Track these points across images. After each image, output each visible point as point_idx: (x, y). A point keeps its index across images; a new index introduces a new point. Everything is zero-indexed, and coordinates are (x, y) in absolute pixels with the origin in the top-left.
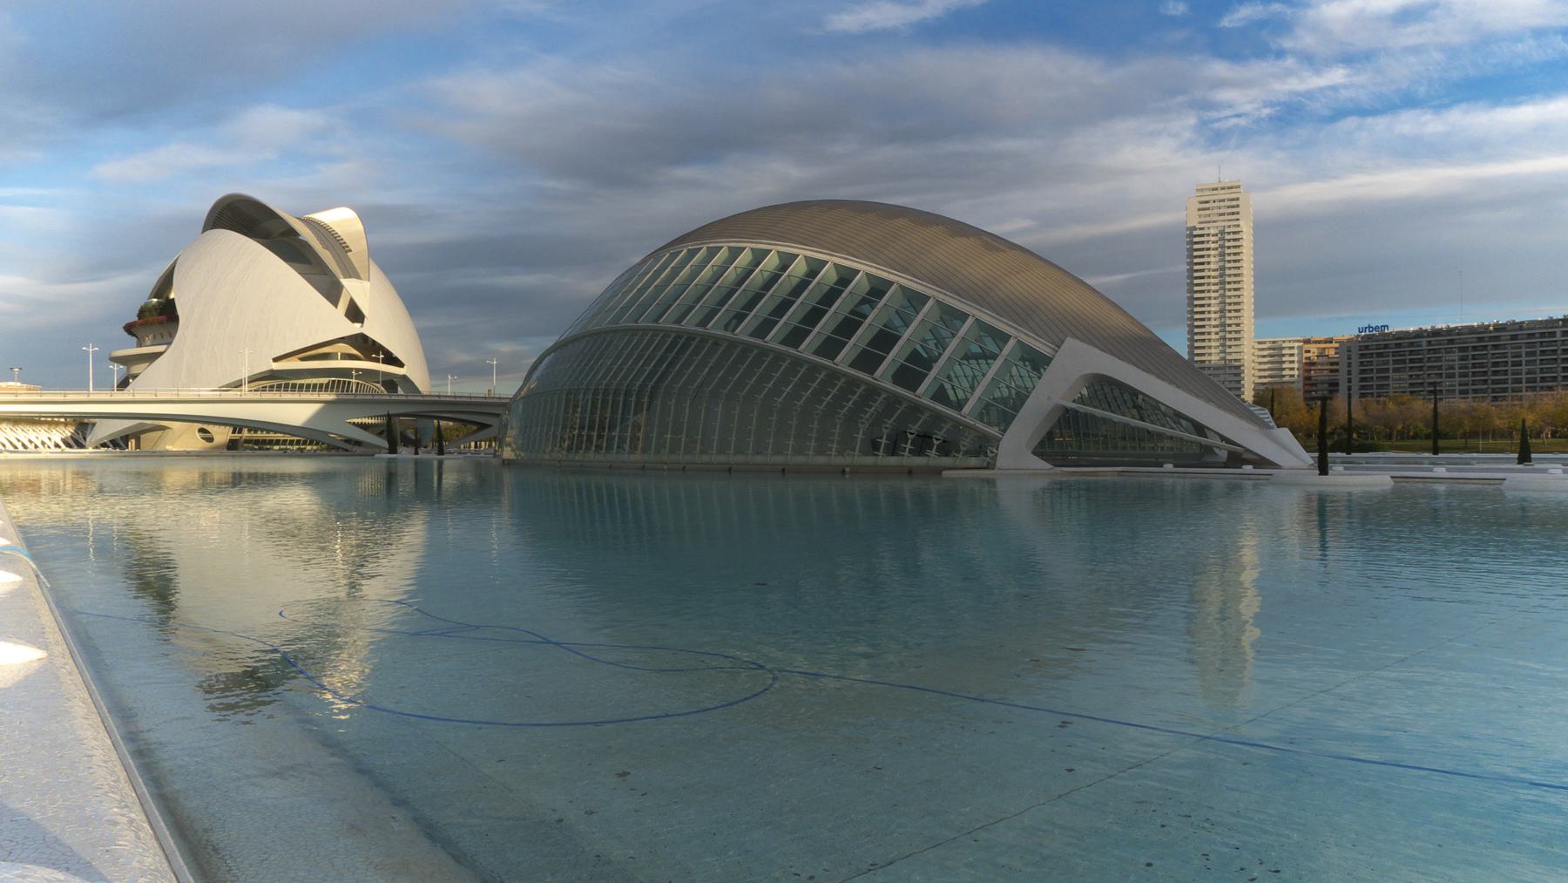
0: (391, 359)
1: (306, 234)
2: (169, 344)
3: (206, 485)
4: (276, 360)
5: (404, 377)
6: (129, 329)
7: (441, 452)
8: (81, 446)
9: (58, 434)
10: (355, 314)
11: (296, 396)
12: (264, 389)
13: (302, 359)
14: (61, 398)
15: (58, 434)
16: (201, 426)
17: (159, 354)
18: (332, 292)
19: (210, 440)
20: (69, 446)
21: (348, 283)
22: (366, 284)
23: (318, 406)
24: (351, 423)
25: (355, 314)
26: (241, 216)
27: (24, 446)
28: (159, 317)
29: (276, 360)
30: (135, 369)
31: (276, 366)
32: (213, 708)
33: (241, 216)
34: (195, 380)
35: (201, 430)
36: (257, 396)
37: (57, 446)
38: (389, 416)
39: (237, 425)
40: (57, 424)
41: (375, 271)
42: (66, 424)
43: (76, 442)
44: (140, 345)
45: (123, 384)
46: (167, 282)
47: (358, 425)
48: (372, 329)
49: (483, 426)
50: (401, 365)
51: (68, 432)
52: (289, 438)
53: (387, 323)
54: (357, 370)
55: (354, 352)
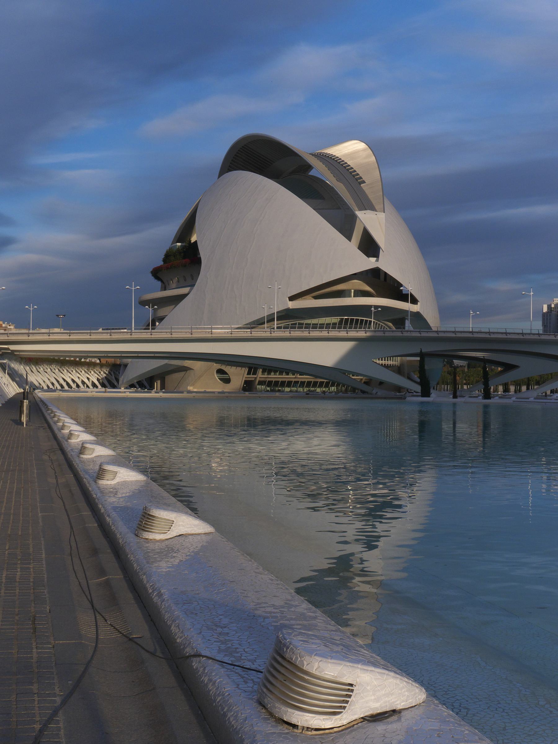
0: (404, 297)
1: (319, 170)
2: (193, 286)
3: (224, 427)
4: (292, 298)
5: (417, 316)
6: (156, 273)
7: (455, 397)
8: (114, 387)
9: (94, 376)
10: (369, 246)
11: (305, 334)
12: (293, 327)
13: (316, 298)
14: (87, 337)
15: (94, 376)
16: (217, 366)
17: (184, 296)
18: (345, 224)
19: (227, 381)
20: (103, 385)
21: (361, 215)
22: (382, 216)
23: (349, 345)
24: (381, 364)
25: (369, 246)
26: (259, 156)
27: (68, 384)
28: (183, 261)
29: (292, 298)
30: (161, 312)
31: (292, 305)
32: (191, 497)
33: (259, 156)
34: (214, 323)
35: (220, 371)
36: (286, 334)
37: (94, 385)
38: (422, 355)
39: (252, 365)
40: (94, 365)
41: (388, 206)
42: (101, 365)
43: (110, 382)
44: (164, 288)
45: (153, 324)
46: (189, 226)
47: (387, 367)
48: (390, 263)
49: (508, 367)
50: (414, 301)
51: (103, 373)
52: (312, 379)
53: (399, 260)
54: (376, 307)
55: (368, 288)
